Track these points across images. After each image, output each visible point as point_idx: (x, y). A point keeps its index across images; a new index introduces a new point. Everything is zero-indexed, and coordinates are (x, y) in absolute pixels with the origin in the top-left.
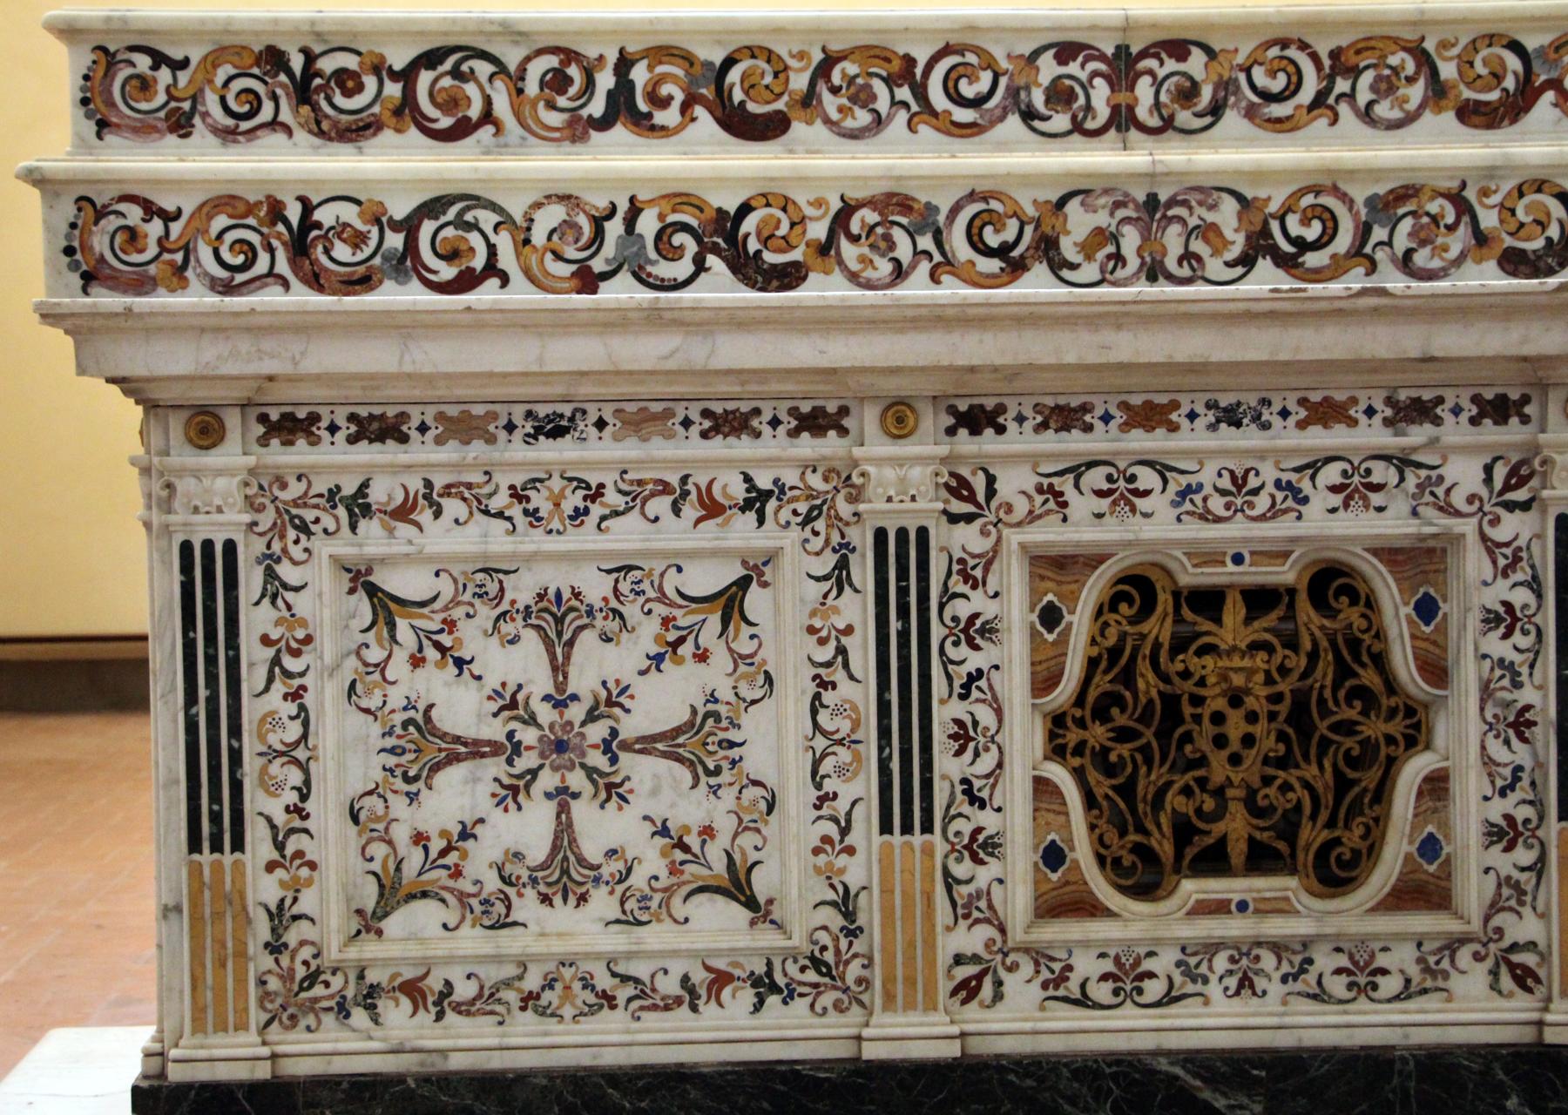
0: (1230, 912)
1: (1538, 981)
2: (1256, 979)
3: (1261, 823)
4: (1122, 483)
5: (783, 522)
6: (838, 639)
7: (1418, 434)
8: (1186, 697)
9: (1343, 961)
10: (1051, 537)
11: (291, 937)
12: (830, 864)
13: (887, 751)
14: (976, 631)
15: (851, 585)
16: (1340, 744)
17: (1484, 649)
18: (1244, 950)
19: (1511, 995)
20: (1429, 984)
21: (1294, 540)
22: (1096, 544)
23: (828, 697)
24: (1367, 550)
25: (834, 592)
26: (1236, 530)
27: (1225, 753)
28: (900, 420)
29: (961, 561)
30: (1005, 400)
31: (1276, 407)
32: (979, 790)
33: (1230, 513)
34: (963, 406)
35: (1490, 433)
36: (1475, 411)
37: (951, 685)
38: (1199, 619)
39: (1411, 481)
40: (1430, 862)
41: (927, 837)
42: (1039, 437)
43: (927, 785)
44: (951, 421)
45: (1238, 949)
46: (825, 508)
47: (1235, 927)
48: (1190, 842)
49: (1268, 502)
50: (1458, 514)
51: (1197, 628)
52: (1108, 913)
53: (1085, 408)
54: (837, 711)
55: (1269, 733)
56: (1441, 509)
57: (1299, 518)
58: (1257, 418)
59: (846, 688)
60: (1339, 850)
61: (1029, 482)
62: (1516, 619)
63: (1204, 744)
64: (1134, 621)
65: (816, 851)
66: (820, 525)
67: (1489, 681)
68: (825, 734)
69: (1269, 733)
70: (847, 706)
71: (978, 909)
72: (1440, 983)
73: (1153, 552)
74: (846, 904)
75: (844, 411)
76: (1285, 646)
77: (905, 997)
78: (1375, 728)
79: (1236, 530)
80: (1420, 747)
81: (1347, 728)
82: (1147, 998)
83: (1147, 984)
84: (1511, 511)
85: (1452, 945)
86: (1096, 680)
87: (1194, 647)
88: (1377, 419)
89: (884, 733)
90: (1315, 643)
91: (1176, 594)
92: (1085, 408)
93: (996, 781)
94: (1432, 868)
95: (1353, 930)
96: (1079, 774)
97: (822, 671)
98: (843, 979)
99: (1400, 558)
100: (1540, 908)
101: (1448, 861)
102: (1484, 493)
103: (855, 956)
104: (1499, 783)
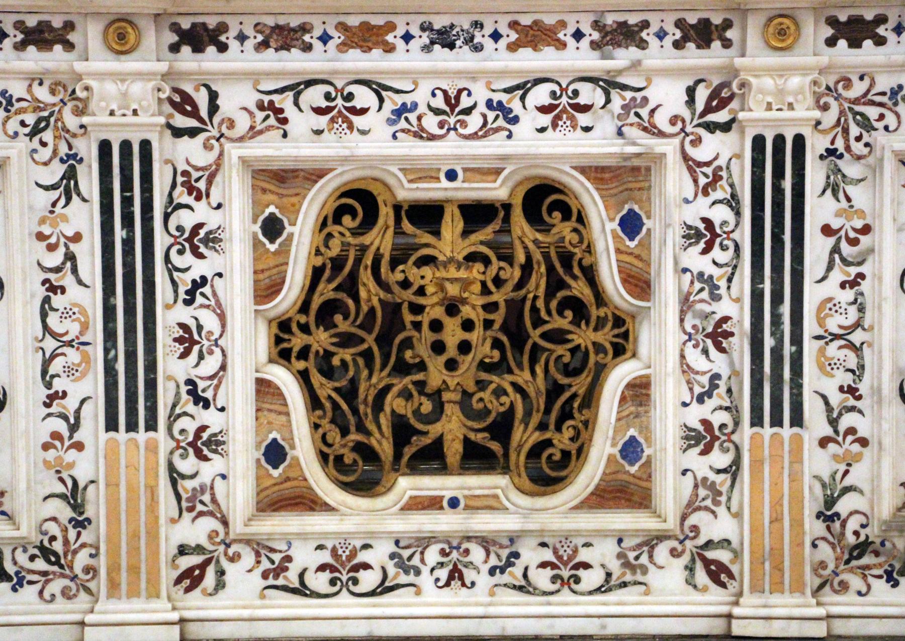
0: (441, 508)
1: (731, 576)
2: (465, 571)
3: (476, 425)
4: (339, 102)
5: (11, 133)
6: (836, 432)
7: (623, 57)
8: (406, 305)
9: (548, 555)
10: (270, 152)
11: (843, 506)
12: (59, 459)
13: (112, 353)
14: (200, 241)
15: (79, 194)
16: (552, 351)
17: (685, 262)
18: (455, 544)
19: (705, 589)
20: (628, 577)
21: (505, 158)
22: (314, 159)
23: (57, 301)
24: (575, 168)
25: (63, 201)
26: (450, 148)
27: (443, 359)
28: (122, 37)
29: (185, 173)
30: (228, 20)
31: (488, 30)
32: (204, 391)
33: (443, 131)
34: (186, 24)
35: (694, 57)
36: (678, 35)
37: (176, 291)
38: (418, 232)
39: (617, 103)
40: (632, 464)
41: (151, 434)
42: (22, 55)
43: (151, 385)
44: (175, 38)
45: (449, 543)
46: (52, 120)
47: (445, 522)
48: (408, 442)
49: (481, 121)
50: (661, 134)
51: (417, 241)
52: (327, 508)
53: (305, 28)
54: (66, 314)
55: (484, 340)
56: (645, 129)
57: (509, 137)
58: (469, 40)
59: (74, 292)
60: (550, 451)
61: (251, 99)
62: (715, 235)
63: (423, 350)
64: (355, 233)
65: (46, 447)
66: (48, 136)
67: (689, 294)
68: (54, 335)
69: (484, 340)
70: (75, 310)
71: (202, 502)
72: (639, 577)
73: (371, 167)
74: (74, 496)
75: (69, 26)
76: (500, 258)
77: (129, 584)
78: (584, 337)
79: (450, 148)
80: (629, 354)
81: (558, 337)
82: (361, 588)
83: (362, 575)
84: (712, 132)
85: (651, 542)
86: (321, 286)
87: (413, 259)
88: (585, 42)
89: (110, 335)
90: (529, 258)
91: (397, 208)
92: (305, 28)
93: (220, 382)
94: (633, 469)
95: (555, 527)
96: (304, 377)
97: (52, 277)
98: (71, 568)
99: (607, 176)
100: (734, 509)
101: (649, 462)
102: (686, 114)
103: (83, 545)
104: (698, 390)
